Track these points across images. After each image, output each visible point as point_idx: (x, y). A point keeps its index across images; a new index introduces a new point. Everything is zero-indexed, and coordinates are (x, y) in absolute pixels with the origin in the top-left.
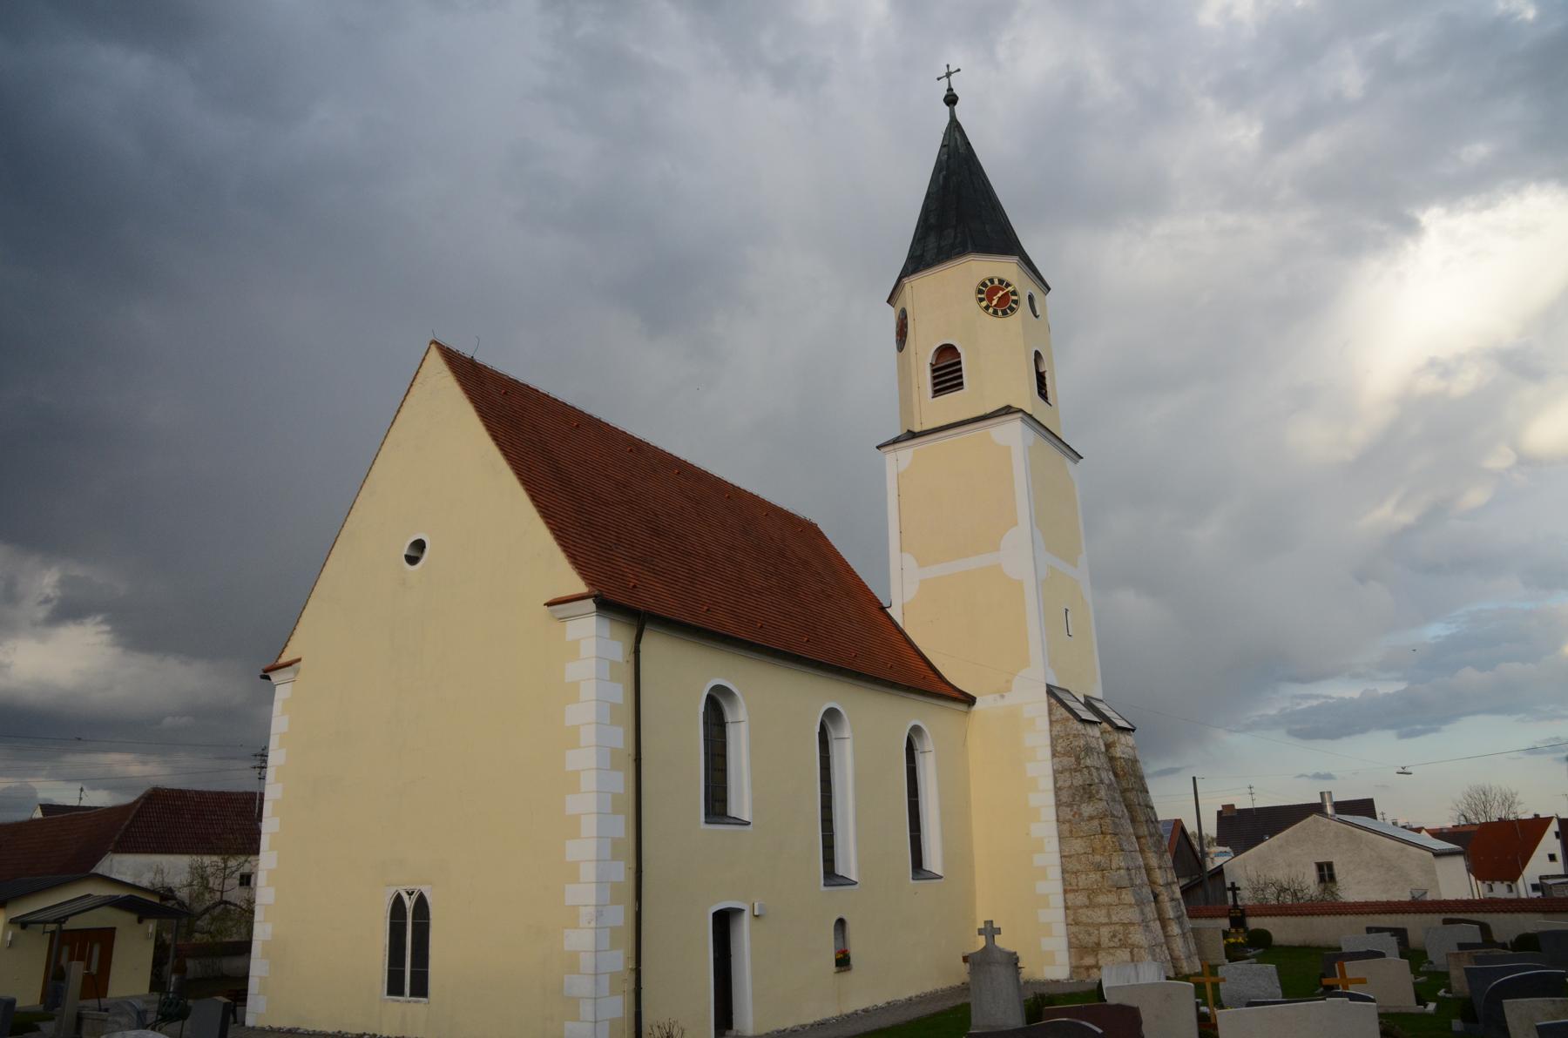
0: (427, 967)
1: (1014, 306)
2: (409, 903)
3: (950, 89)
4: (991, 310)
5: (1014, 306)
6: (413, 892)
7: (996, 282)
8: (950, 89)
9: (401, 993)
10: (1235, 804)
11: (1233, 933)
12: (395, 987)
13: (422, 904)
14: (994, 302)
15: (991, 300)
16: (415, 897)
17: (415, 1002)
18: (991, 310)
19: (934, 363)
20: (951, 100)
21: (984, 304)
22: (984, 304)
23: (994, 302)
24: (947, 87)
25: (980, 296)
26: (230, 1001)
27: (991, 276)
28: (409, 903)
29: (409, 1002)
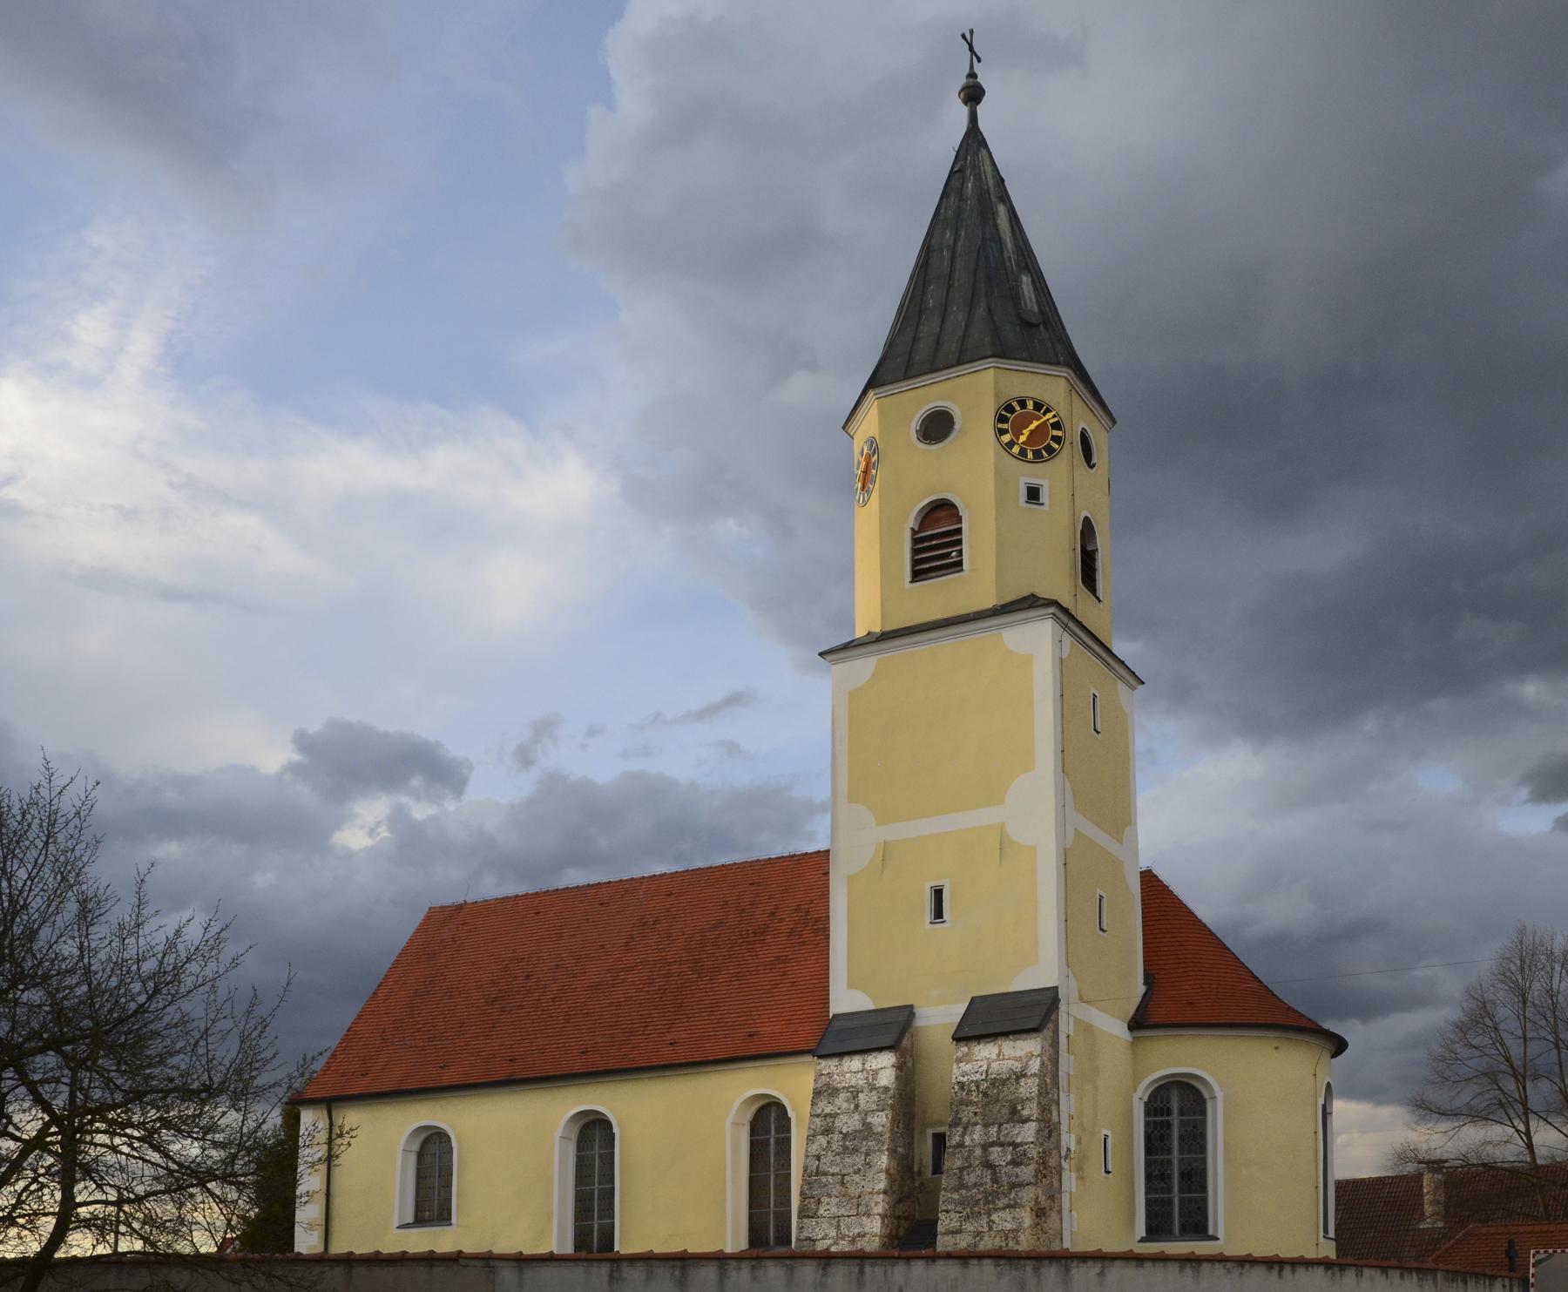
4: (1016, 450)
14: (1023, 438)
15: (1018, 434)
18: (1016, 450)
20: (973, 94)
21: (1006, 438)
22: (1006, 438)
23: (1023, 438)
24: (967, 71)
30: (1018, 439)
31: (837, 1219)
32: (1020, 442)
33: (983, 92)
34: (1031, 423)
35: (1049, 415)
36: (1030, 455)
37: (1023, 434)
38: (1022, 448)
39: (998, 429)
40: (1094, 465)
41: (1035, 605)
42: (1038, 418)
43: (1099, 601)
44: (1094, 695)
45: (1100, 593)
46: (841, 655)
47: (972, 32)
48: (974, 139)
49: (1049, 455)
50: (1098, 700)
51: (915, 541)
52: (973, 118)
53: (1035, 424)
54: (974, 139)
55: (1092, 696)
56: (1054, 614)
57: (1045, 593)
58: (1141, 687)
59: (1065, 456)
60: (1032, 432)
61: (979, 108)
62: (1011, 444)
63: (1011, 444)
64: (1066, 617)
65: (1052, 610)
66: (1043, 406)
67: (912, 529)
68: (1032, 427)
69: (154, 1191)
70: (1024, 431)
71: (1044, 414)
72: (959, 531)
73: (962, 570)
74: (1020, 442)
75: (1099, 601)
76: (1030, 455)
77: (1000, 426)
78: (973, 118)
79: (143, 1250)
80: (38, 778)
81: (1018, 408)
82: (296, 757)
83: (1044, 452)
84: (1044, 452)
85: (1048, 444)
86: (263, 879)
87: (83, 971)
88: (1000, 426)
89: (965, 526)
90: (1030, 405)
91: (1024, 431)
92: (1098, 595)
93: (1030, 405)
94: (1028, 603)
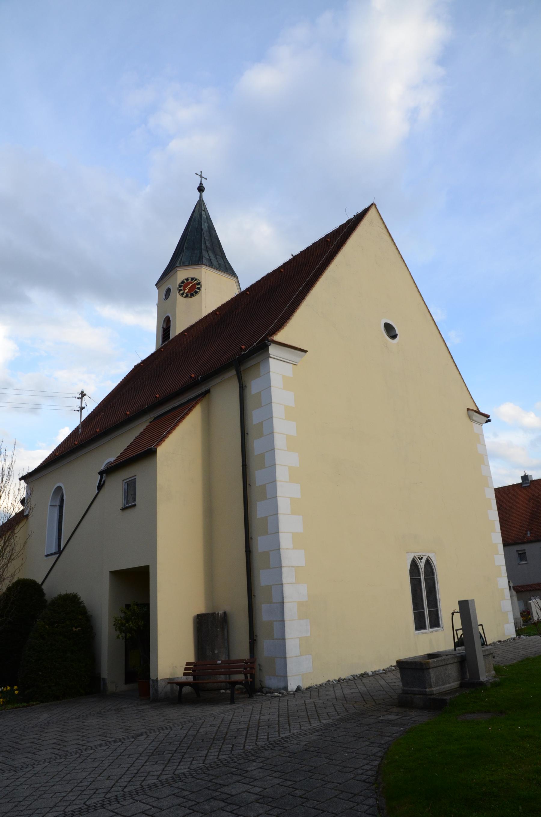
0: (414, 613)
1: (198, 290)
2: (422, 565)
3: (201, 184)
4: (185, 295)
5: (198, 290)
6: (422, 558)
7: (190, 280)
8: (201, 184)
9: (424, 627)
10: (301, 685)
11: (376, 802)
12: (420, 625)
13: (428, 564)
14: (187, 291)
15: (185, 290)
16: (424, 560)
17: (436, 631)
18: (185, 295)
19: (165, 327)
20: (201, 189)
21: (181, 292)
22: (181, 292)
23: (187, 291)
24: (200, 183)
25: (179, 289)
26: (243, 687)
27: (186, 277)
28: (422, 565)
29: (432, 632)
35: (196, 282)
46: (37, 476)
47: (201, 172)
48: (200, 204)
52: (201, 197)
54: (200, 204)
58: (121, 506)
62: (183, 294)
63: (183, 294)
68: (189, 286)
71: (194, 281)
73: (473, 601)
78: (201, 197)
79: (227, 659)
80: (51, 599)
82: (45, 598)
86: (45, 715)
91: (186, 288)
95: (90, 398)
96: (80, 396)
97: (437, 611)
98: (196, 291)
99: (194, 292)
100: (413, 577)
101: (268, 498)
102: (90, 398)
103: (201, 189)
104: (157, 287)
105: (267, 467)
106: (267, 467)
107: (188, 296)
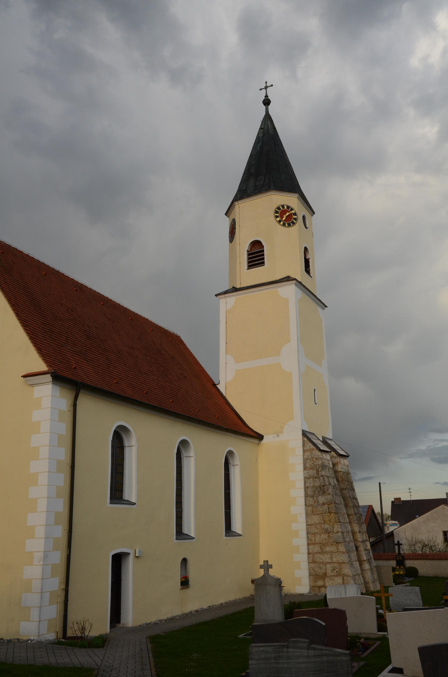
4: (282, 223)
14: (284, 219)
15: (282, 217)
18: (282, 223)
20: (267, 102)
22: (278, 219)
23: (284, 219)
24: (265, 95)
30: (282, 219)
31: (106, 650)
32: (283, 220)
33: (270, 102)
34: (286, 213)
36: (287, 225)
37: (284, 217)
38: (284, 222)
39: (275, 216)
40: (308, 227)
41: (289, 280)
42: (289, 212)
43: (311, 277)
44: (314, 389)
45: (311, 274)
48: (268, 118)
49: (293, 225)
50: (316, 391)
51: (249, 255)
53: (288, 214)
54: (268, 118)
55: (314, 390)
56: (295, 283)
57: (293, 276)
59: (297, 226)
60: (287, 216)
61: (269, 107)
62: (280, 221)
64: (300, 284)
65: (295, 282)
66: (290, 207)
67: (247, 251)
69: (422, 548)
70: (284, 216)
72: (263, 251)
74: (283, 220)
75: (311, 277)
76: (287, 225)
77: (276, 215)
81: (282, 208)
83: (291, 224)
84: (291, 224)
85: (292, 221)
87: (324, 546)
88: (276, 215)
89: (265, 249)
90: (286, 207)
91: (284, 216)
92: (311, 275)
93: (286, 207)
94: (288, 279)
95: (185, 583)
96: (364, 542)
97: (230, 493)
98: (292, 221)
99: (291, 222)
100: (181, 511)
101: (49, 593)
102: (185, 583)
103: (267, 102)
104: (227, 217)
105: (50, 564)
106: (50, 564)
107: (296, 218)
